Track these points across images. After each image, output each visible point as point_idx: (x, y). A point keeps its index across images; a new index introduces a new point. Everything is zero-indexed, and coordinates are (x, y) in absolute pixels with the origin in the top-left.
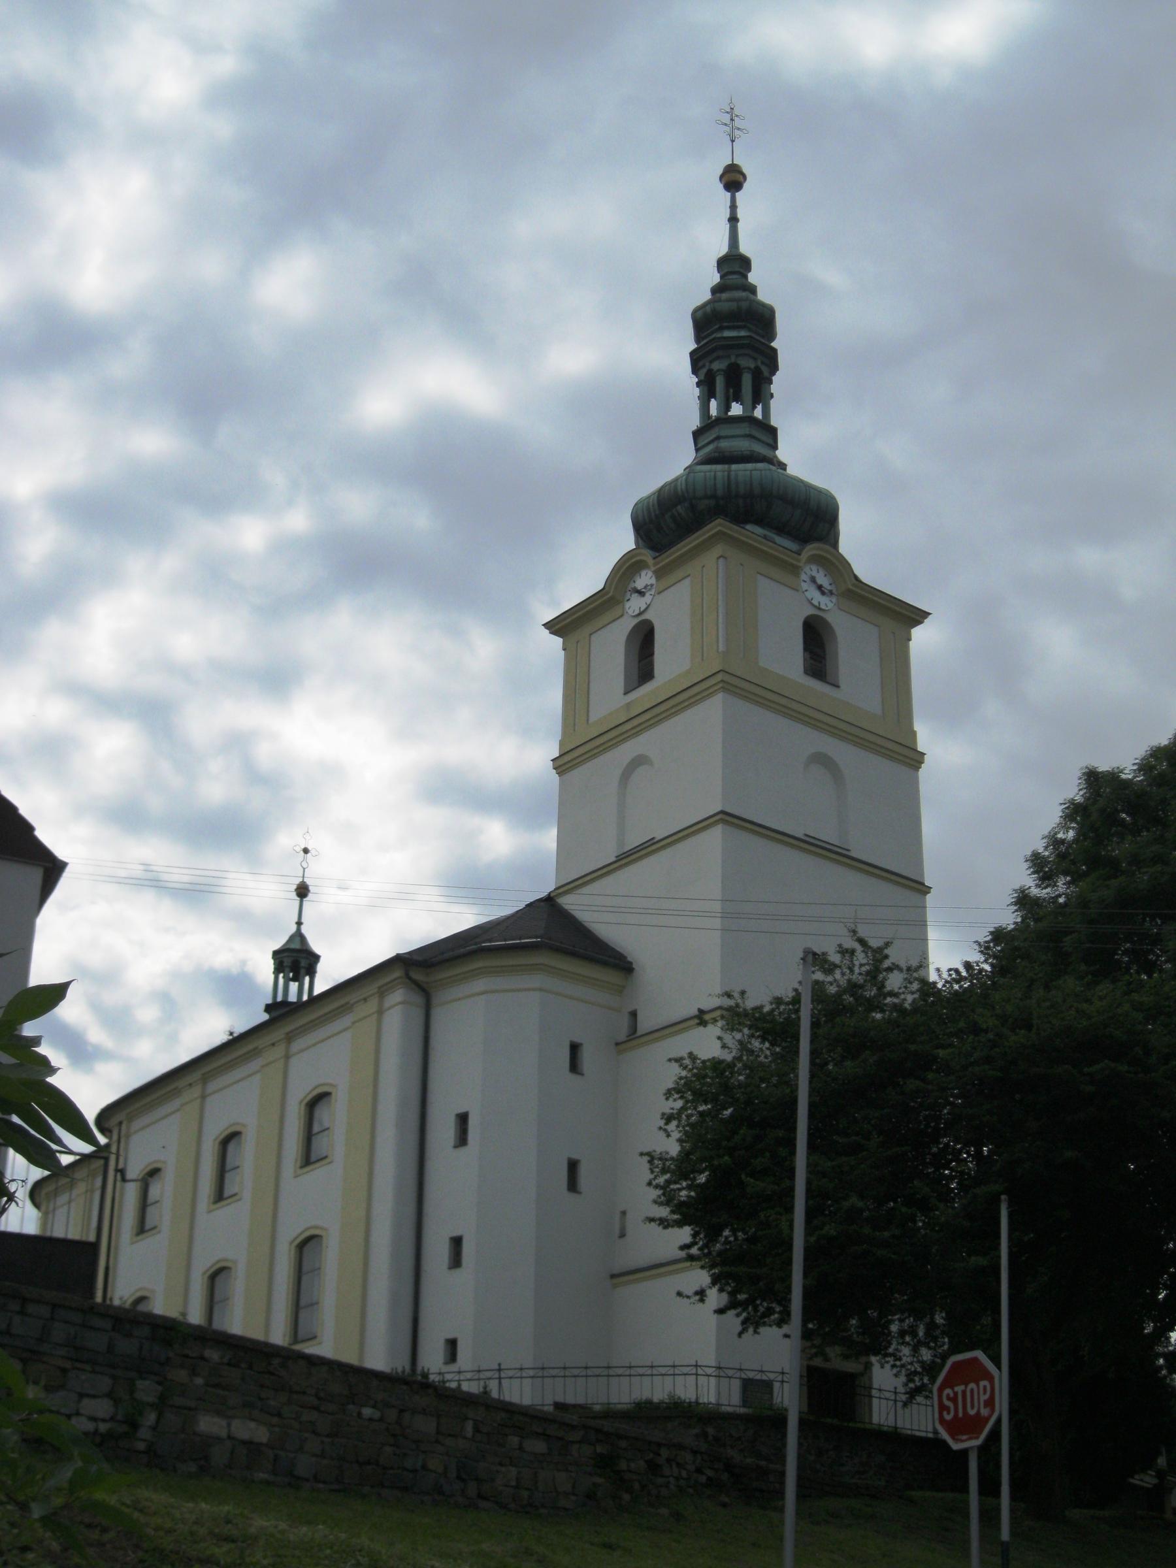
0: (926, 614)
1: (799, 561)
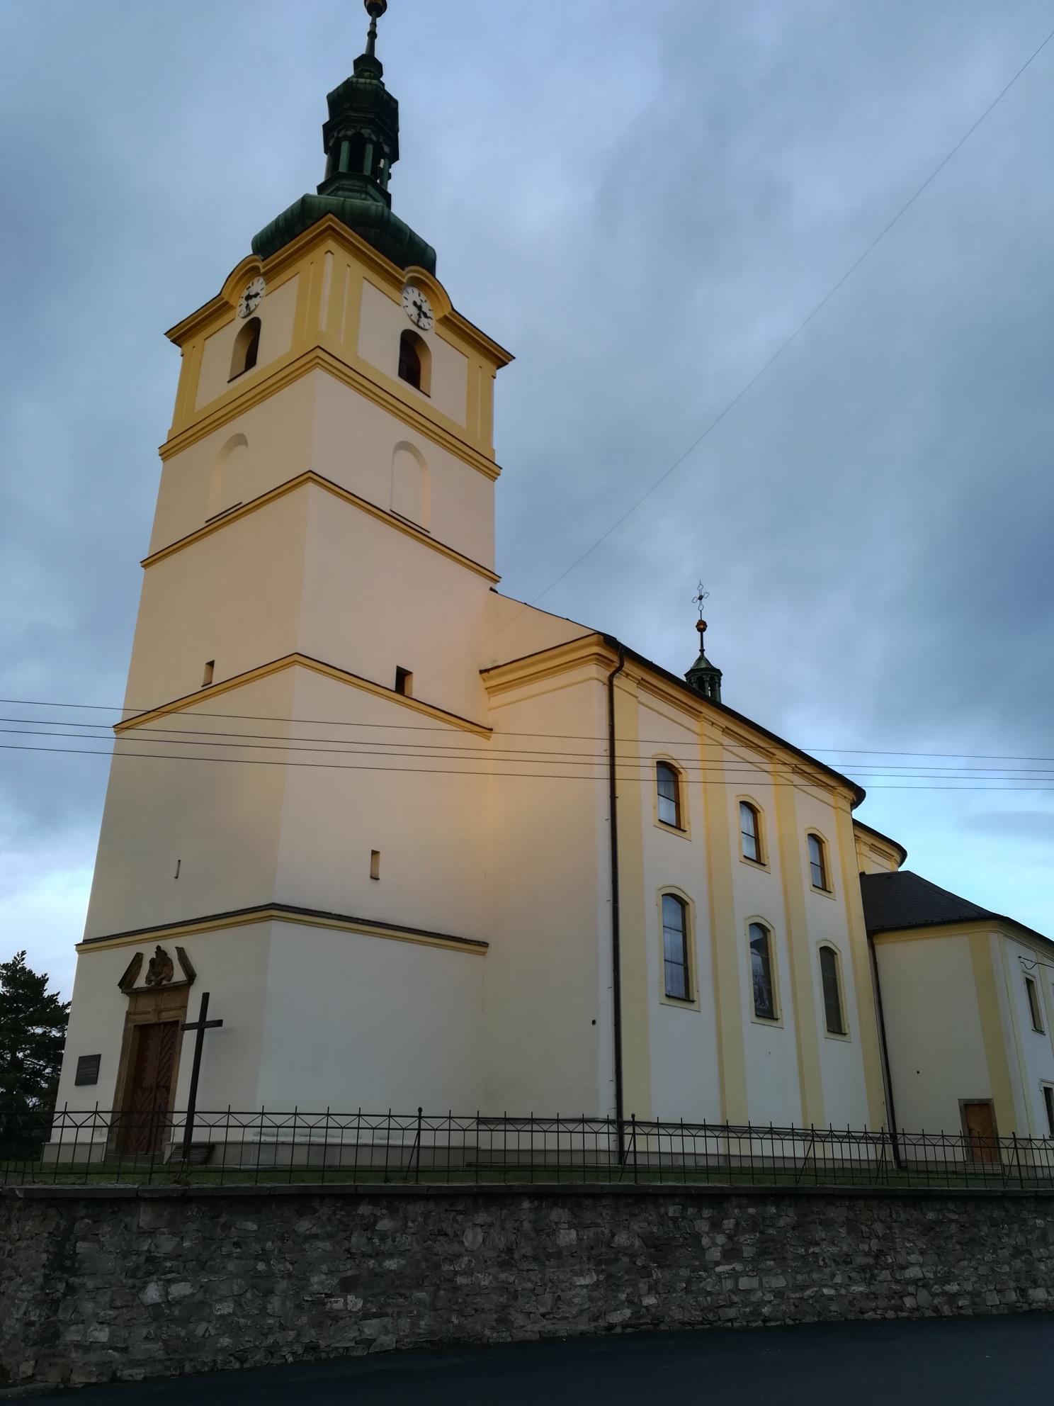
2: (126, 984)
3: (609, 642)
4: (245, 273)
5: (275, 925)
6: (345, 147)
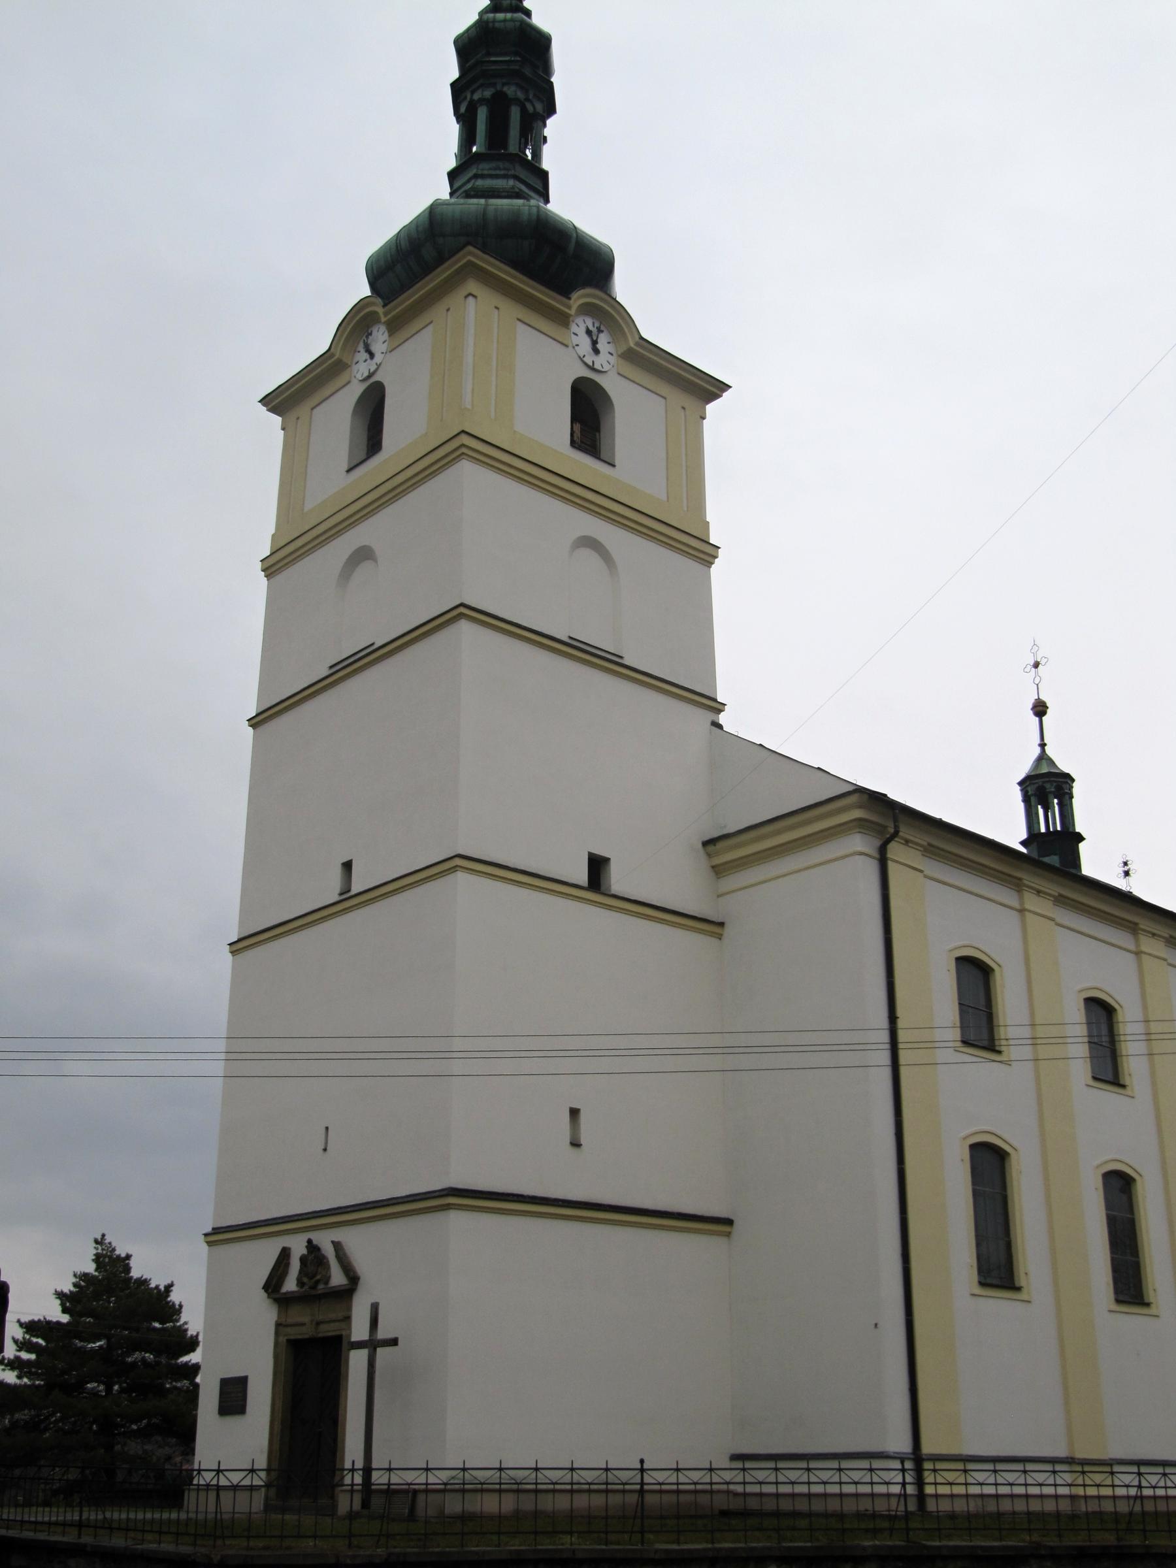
0: (724, 387)
1: (569, 307)
2: (272, 1286)
3: (878, 800)
4: (356, 327)
5: (454, 1216)
6: (482, 114)
